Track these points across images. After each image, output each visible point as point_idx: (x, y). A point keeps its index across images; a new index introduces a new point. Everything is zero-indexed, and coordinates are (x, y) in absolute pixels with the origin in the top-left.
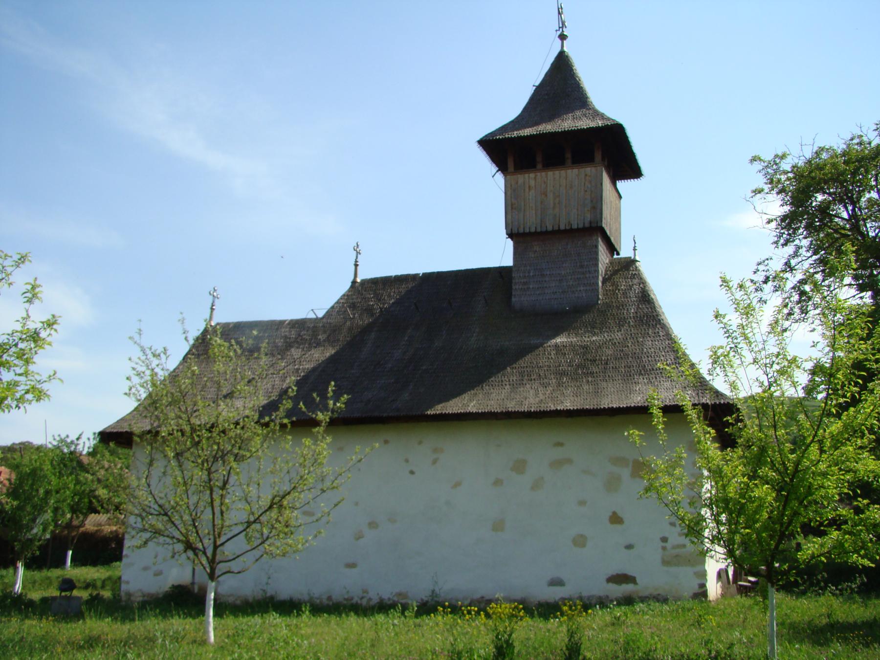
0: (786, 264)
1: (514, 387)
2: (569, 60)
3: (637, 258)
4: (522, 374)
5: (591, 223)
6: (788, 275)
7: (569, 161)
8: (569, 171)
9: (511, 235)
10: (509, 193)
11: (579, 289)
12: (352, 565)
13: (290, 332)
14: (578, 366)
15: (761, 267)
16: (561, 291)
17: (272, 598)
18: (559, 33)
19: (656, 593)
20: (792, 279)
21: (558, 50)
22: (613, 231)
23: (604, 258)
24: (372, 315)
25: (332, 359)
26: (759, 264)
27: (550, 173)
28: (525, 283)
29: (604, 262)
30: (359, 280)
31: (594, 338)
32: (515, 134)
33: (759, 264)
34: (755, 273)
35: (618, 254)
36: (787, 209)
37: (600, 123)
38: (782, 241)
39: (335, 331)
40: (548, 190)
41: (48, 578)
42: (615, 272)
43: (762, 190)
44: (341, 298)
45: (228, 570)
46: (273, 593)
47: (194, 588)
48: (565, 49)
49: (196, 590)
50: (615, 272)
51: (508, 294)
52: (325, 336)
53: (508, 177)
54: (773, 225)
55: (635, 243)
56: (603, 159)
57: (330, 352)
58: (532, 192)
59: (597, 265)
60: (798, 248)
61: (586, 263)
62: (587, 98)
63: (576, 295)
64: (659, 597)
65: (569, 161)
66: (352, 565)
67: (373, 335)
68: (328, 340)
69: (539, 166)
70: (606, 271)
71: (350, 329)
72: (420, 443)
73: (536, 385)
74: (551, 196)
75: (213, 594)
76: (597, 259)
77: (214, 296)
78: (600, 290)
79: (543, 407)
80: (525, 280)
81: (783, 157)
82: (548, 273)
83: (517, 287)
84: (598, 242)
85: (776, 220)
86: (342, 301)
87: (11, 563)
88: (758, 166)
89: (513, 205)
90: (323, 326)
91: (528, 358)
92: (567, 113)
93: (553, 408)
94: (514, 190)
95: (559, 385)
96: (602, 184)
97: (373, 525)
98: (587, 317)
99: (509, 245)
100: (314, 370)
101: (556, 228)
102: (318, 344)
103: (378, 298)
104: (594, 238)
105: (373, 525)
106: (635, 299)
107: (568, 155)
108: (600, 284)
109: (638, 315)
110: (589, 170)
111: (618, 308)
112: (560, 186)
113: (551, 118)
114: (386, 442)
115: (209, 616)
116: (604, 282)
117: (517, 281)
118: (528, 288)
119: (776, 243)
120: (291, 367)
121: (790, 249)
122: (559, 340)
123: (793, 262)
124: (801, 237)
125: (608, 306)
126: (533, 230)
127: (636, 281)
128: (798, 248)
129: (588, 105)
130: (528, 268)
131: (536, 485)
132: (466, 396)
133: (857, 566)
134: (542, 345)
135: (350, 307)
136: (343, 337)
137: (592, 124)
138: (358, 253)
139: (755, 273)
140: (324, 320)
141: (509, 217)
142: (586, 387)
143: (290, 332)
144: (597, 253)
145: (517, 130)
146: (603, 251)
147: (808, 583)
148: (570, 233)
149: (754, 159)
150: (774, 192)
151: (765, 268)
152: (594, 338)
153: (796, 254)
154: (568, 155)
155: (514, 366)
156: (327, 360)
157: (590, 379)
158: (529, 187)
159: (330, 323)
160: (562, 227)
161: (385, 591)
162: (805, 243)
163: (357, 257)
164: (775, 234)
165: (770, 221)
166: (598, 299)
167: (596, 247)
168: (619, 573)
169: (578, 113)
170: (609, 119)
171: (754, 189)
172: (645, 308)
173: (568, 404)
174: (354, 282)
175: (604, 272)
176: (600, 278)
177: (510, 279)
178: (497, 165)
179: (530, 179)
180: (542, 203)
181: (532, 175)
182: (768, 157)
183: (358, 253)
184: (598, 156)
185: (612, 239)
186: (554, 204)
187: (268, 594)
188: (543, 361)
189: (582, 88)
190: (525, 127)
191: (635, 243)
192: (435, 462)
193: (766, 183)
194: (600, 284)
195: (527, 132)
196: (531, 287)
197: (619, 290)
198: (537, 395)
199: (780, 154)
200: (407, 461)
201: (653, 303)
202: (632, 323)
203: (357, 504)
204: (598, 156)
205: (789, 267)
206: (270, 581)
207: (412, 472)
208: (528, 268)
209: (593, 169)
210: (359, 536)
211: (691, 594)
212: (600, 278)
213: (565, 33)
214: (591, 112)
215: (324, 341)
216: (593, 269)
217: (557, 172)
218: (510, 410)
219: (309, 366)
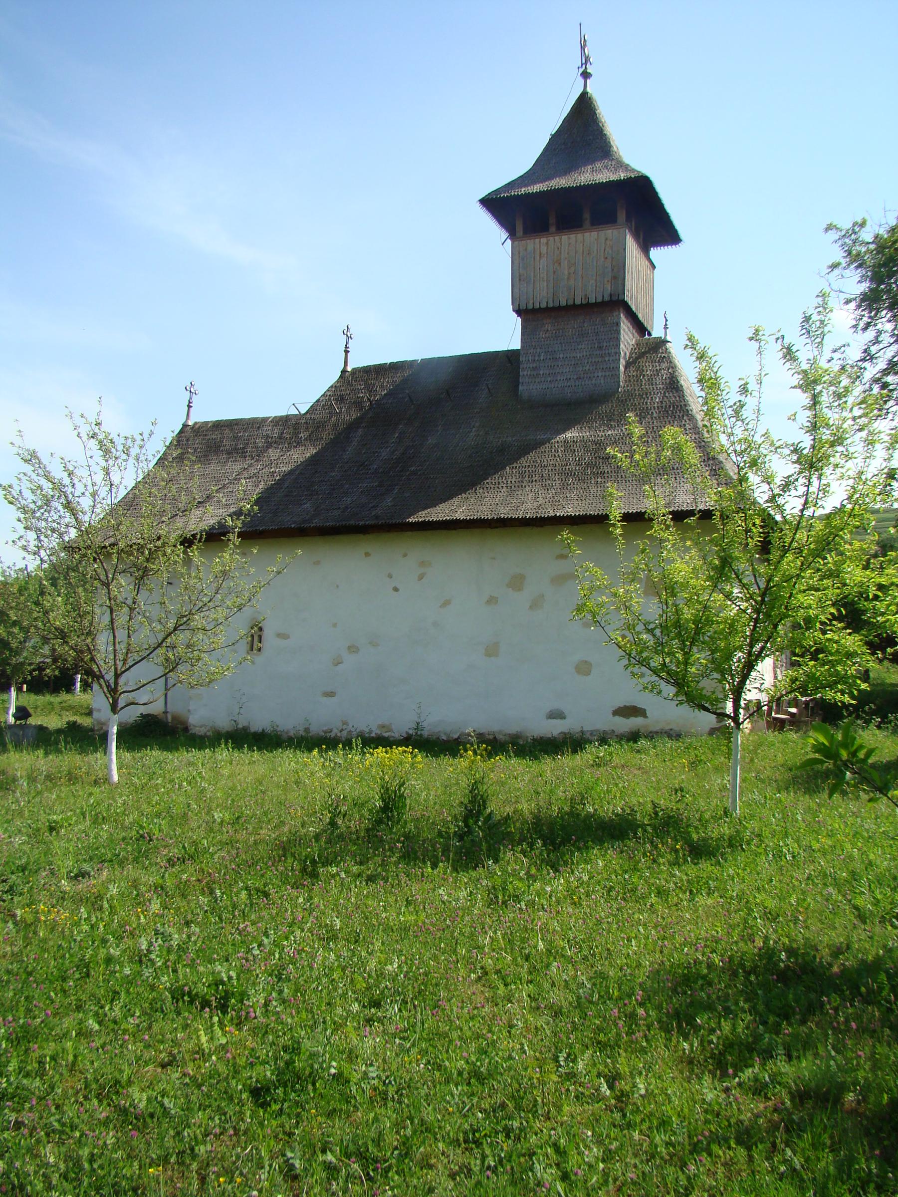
0: (865, 351)
1: (511, 490)
2: (592, 102)
3: (668, 339)
4: (522, 475)
5: (611, 295)
6: (867, 364)
7: (587, 223)
8: (587, 235)
9: (519, 312)
10: (516, 262)
11: (596, 375)
12: (331, 694)
13: (273, 430)
14: (588, 465)
15: (836, 356)
16: (575, 377)
17: (245, 729)
18: (581, 70)
19: (667, 728)
20: (871, 371)
21: (581, 90)
22: (641, 306)
23: (628, 338)
24: (361, 410)
25: (313, 461)
26: (835, 351)
27: (565, 238)
28: (534, 369)
29: (628, 343)
30: (349, 369)
31: (610, 433)
32: (523, 191)
33: (835, 351)
34: (829, 361)
35: (650, 334)
36: (865, 286)
37: (622, 175)
38: (862, 324)
39: (318, 427)
40: (563, 257)
41: (51, 703)
42: (642, 355)
43: (839, 264)
44: (328, 390)
45: (132, 700)
46: (245, 724)
47: (167, 718)
48: (589, 90)
49: (170, 719)
50: (642, 355)
51: (515, 383)
52: (307, 434)
53: (516, 243)
54: (853, 305)
55: (667, 320)
56: (628, 219)
57: (311, 451)
58: (544, 260)
59: (618, 346)
60: (879, 333)
61: (605, 344)
62: (611, 146)
63: (593, 382)
64: (671, 732)
65: (587, 223)
66: (331, 694)
67: (360, 432)
68: (309, 438)
69: (553, 229)
70: (631, 354)
71: (335, 425)
72: (405, 555)
73: (537, 487)
74: (565, 264)
75: (115, 727)
76: (618, 340)
77: (191, 390)
78: (622, 376)
79: (541, 514)
80: (534, 365)
81: (863, 225)
82: (561, 356)
83: (525, 373)
84: (619, 318)
85: (855, 299)
86: (328, 393)
87: (5, 688)
88: (833, 235)
89: (519, 278)
90: (305, 423)
91: (531, 456)
92: (585, 165)
93: (552, 514)
94: (523, 259)
95: (563, 487)
96: (625, 249)
97: (353, 649)
98: (604, 408)
99: (515, 323)
100: (291, 472)
101: (571, 302)
102: (299, 444)
103: (370, 389)
104: (615, 314)
105: (353, 649)
106: (662, 386)
107: (587, 216)
108: (622, 368)
109: (664, 405)
110: (610, 233)
111: (641, 396)
112: (576, 252)
113: (566, 172)
114: (367, 554)
115: (111, 753)
116: (626, 368)
117: (525, 366)
118: (538, 375)
119: (855, 326)
120: (266, 470)
121: (871, 334)
122: (569, 435)
123: (873, 349)
124: (884, 320)
125: (629, 394)
126: (544, 305)
127: (664, 365)
128: (879, 333)
129: (611, 155)
130: (538, 350)
131: (536, 604)
132: (456, 501)
133: (836, 703)
134: (549, 440)
135: (336, 400)
136: (327, 435)
137: (613, 177)
138: (349, 338)
139: (829, 361)
140: (308, 416)
141: (516, 290)
142: (593, 489)
143: (273, 430)
144: (618, 332)
145: (526, 186)
146: (627, 330)
147: (854, 716)
148: (587, 308)
149: (829, 228)
150: (852, 267)
151: (842, 357)
152: (610, 433)
153: (876, 341)
154: (587, 216)
155: (515, 465)
156: (306, 461)
157: (599, 480)
158: (540, 254)
159: (314, 419)
160: (578, 302)
161: (369, 724)
162: (889, 327)
163: (347, 343)
164: (853, 316)
165: (848, 302)
166: (619, 386)
167: (618, 324)
168: (628, 704)
169: (598, 165)
170: (633, 170)
171: (830, 264)
172: (672, 397)
173: (570, 510)
174: (344, 371)
175: (628, 354)
176: (622, 362)
177: (518, 363)
178: (508, 230)
179: (541, 244)
180: (554, 272)
181: (544, 240)
182: (847, 225)
183: (349, 338)
184: (622, 216)
185: (640, 316)
186: (569, 274)
187: (240, 726)
188: (548, 460)
189: (605, 135)
190: (535, 183)
191: (667, 320)
192: (421, 577)
193: (844, 257)
194: (622, 368)
195: (537, 188)
196: (541, 372)
197: (644, 376)
198: (536, 499)
199: (860, 221)
200: (390, 576)
201: (682, 391)
202: (655, 415)
203: (335, 625)
204: (622, 216)
205: (868, 356)
206: (242, 711)
207: (396, 589)
208: (538, 350)
209: (615, 232)
210: (338, 662)
211: (707, 729)
212: (622, 362)
213: (589, 71)
214: (613, 163)
215: (306, 439)
216: (613, 351)
217: (572, 236)
218: (502, 516)
219: (285, 469)
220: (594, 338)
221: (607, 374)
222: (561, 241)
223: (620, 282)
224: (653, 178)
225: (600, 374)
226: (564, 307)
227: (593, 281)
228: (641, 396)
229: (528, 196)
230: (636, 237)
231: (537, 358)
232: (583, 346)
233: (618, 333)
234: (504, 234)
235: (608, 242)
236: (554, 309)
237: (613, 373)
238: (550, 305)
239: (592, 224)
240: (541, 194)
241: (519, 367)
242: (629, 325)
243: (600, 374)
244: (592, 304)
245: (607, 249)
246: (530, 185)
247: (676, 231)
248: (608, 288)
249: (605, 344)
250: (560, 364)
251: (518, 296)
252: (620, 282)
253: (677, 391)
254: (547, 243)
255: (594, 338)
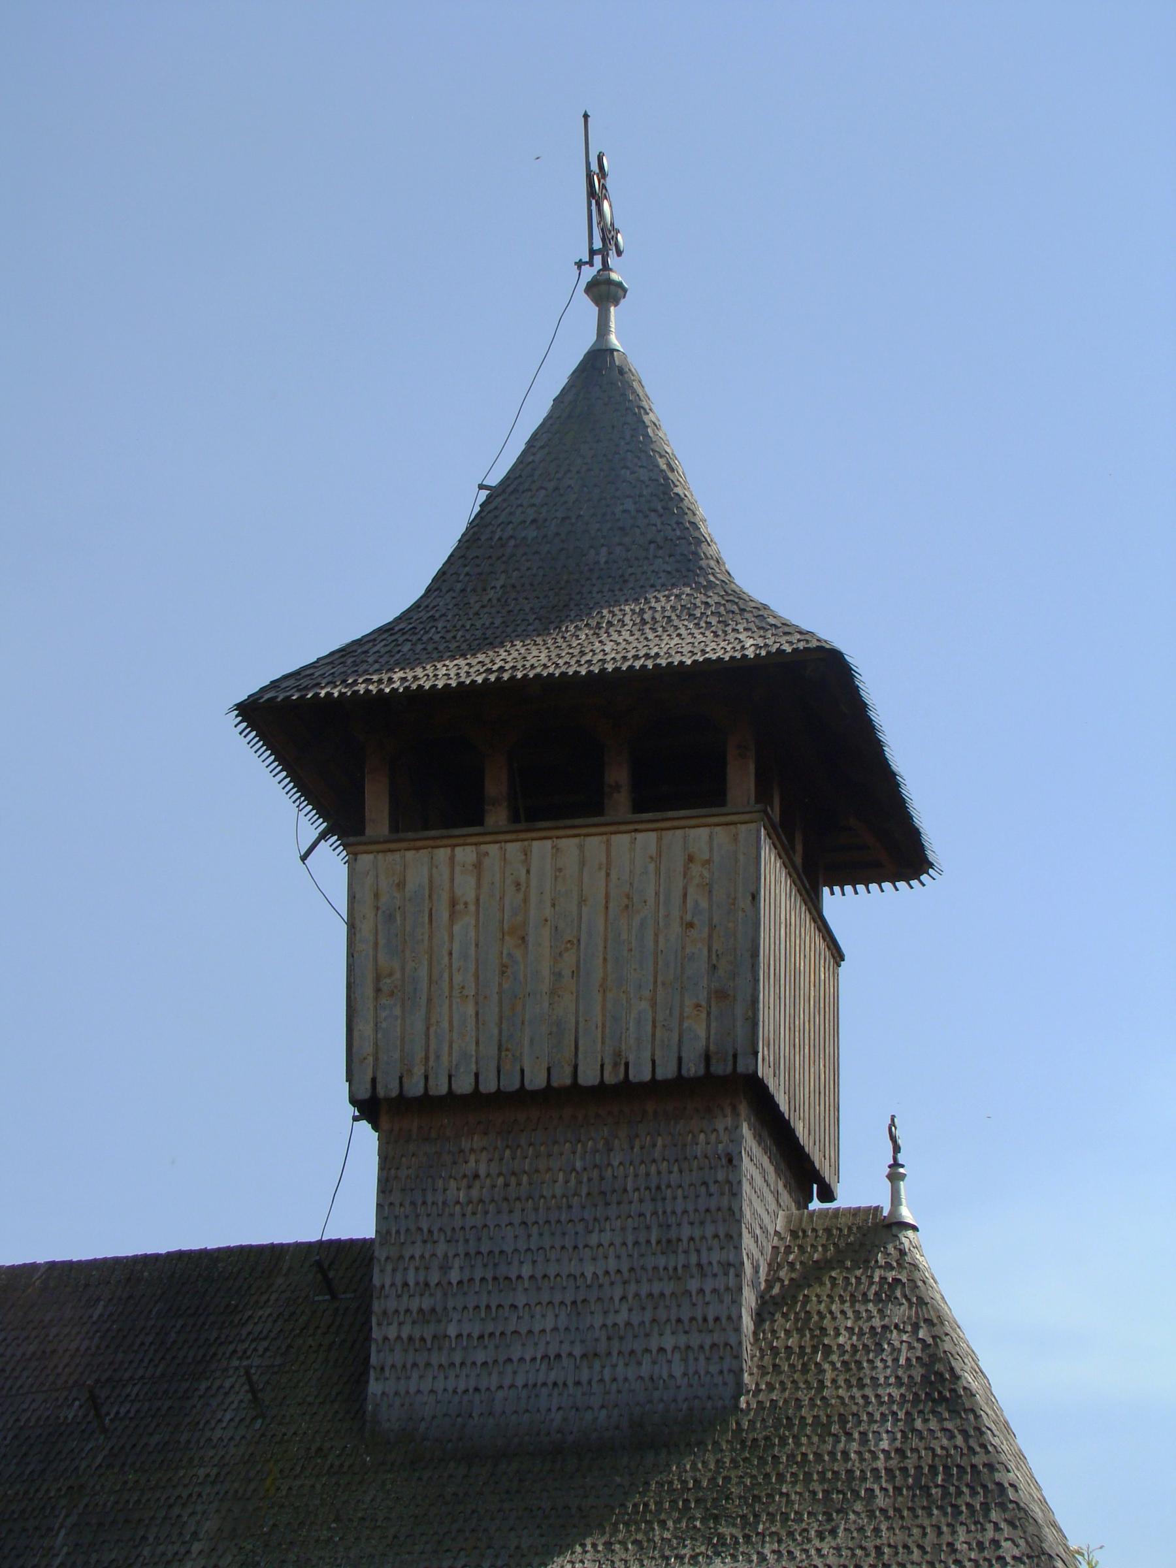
3: (906, 1214)
5: (707, 1058)
10: (366, 929)
16: (578, 1351)
18: (589, 273)
21: (588, 340)
27: (541, 848)
32: (398, 680)
35: (827, 1194)
37: (750, 645)
42: (814, 1273)
50: (814, 1273)
53: (366, 859)
55: (897, 1149)
56: (763, 794)
59: (732, 1240)
61: (686, 1231)
62: (700, 541)
63: (645, 1369)
65: (621, 801)
69: (497, 817)
70: (774, 1266)
76: (734, 1216)
80: (426, 1304)
82: (526, 1271)
84: (737, 1141)
94: (390, 918)
96: (755, 897)
101: (562, 1079)
107: (618, 775)
108: (747, 1323)
109: (910, 1464)
112: (582, 901)
116: (759, 1318)
117: (392, 1304)
126: (464, 1085)
127: (899, 1313)
130: (441, 1248)
137: (719, 649)
141: (365, 1028)
146: (759, 1180)
154: (618, 775)
158: (453, 903)
160: (588, 1077)
167: (732, 1161)
169: (661, 603)
170: (786, 628)
176: (749, 1298)
177: (365, 1295)
178: (322, 811)
181: (466, 854)
190: (438, 654)
191: (897, 1149)
194: (747, 1323)
196: (452, 1331)
197: (828, 1350)
202: (881, 1501)
208: (441, 1248)
212: (749, 1298)
216: (715, 1257)
217: (569, 845)
220: (648, 1208)
221: (695, 1340)
222: (526, 861)
223: (740, 1010)
224: (855, 657)
225: (669, 1342)
226: (535, 1094)
227: (645, 1005)
228: (820, 1425)
229: (417, 698)
230: (785, 852)
231: (434, 1278)
232: (606, 1238)
233: (734, 1191)
234: (309, 825)
235: (696, 869)
236: (500, 1099)
237: (717, 1337)
238: (489, 1085)
239: (642, 804)
240: (464, 694)
241: (368, 1312)
242: (766, 1161)
243: (669, 1342)
244: (642, 1085)
245: (691, 891)
246: (418, 662)
247: (914, 835)
248: (699, 1030)
249: (686, 1231)
250: (521, 1300)
251: (368, 1049)
252: (740, 1010)
253: (955, 1413)
254: (478, 866)
255: (648, 1208)
